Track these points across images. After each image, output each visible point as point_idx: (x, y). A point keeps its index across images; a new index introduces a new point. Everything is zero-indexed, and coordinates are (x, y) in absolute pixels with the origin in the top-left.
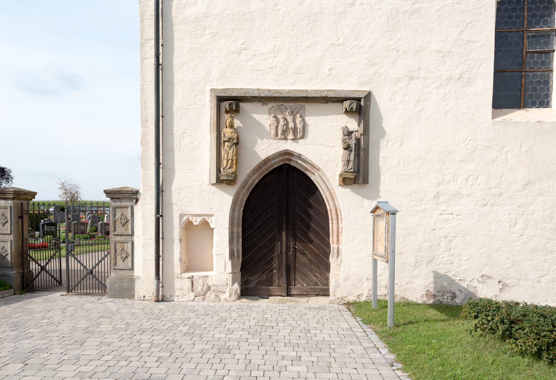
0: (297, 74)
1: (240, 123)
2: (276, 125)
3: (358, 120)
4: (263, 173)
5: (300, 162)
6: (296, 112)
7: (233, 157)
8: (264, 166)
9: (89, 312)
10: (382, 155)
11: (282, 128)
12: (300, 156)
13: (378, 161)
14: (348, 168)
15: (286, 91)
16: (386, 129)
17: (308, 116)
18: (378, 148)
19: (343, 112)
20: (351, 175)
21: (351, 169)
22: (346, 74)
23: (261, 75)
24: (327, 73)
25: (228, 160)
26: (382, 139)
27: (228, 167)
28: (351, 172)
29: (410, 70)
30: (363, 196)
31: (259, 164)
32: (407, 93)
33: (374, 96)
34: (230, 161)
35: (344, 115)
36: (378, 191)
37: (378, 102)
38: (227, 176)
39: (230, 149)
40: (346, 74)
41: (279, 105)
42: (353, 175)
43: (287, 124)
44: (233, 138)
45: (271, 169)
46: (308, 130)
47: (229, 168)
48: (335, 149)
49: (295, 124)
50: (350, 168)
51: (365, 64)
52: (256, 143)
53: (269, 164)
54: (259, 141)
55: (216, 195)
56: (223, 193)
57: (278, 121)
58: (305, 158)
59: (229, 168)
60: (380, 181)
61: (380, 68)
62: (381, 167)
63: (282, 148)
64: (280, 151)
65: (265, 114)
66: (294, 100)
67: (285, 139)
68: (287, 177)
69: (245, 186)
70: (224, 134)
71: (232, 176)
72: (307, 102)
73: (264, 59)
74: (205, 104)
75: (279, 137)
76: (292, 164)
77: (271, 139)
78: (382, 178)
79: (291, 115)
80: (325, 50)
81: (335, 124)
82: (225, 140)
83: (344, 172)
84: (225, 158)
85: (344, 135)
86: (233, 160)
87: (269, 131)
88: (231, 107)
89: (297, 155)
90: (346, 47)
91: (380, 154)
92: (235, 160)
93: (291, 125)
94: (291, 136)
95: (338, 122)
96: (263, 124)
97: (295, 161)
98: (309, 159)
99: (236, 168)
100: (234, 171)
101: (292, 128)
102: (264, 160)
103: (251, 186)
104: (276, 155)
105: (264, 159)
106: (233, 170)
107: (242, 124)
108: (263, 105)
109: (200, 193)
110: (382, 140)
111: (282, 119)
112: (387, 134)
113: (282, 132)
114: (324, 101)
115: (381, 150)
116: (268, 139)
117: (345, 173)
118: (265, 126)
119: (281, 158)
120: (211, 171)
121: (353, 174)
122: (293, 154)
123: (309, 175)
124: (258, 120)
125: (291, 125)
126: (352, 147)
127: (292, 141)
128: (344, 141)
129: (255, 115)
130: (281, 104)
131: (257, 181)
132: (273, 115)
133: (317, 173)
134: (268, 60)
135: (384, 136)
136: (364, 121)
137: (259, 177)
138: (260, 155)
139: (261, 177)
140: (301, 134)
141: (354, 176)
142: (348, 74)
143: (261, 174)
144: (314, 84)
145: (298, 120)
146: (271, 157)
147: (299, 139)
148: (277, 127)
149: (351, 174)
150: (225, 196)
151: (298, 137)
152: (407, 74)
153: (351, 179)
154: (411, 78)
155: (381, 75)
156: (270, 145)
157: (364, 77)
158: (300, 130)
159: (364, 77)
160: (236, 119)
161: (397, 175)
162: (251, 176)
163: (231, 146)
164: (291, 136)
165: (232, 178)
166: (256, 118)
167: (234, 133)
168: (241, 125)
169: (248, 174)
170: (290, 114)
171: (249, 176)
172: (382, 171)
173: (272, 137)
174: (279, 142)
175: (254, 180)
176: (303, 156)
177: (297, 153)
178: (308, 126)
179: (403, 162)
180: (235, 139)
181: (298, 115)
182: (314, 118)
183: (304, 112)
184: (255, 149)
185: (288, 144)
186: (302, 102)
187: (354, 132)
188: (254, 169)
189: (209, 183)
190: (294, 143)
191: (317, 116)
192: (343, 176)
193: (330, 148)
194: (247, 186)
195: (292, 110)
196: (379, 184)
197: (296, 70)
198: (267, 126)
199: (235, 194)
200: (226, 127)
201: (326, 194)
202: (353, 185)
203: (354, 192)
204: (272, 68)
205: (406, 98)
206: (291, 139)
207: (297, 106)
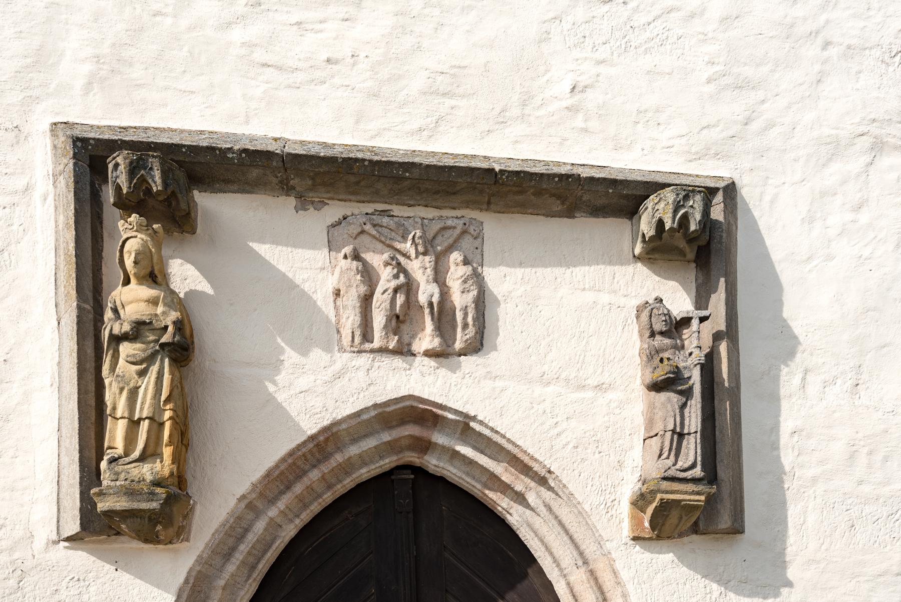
0: (444, 95)
1: (201, 278)
2: (363, 289)
3: (694, 285)
4: (316, 499)
5: (466, 451)
6: (446, 244)
7: (158, 409)
8: (314, 466)
9: (854, 447)
10: (787, 425)
11: (387, 305)
12: (467, 425)
13: (775, 446)
14: (680, 464)
15: (401, 152)
16: (797, 328)
17: (493, 266)
18: (774, 399)
19: (638, 250)
20: (693, 493)
21: (693, 466)
22: (639, 112)
23: (289, 86)
24: (565, 104)
25: (134, 424)
26: (787, 366)
27: (136, 454)
28: (694, 480)
29: (872, 116)
30: (724, 582)
31: (291, 454)
32: (867, 200)
33: (746, 204)
34: (145, 425)
35: (639, 265)
36: (780, 563)
37: (761, 228)
38: (130, 492)
39: (142, 373)
40: (639, 112)
41: (370, 211)
42: (698, 493)
43: (408, 288)
44: (156, 324)
45: (348, 483)
46: (498, 320)
47: (142, 459)
48: (611, 395)
49: (445, 293)
50: (689, 463)
51: (709, 81)
52: (276, 365)
53: (339, 458)
54: (290, 356)
55: (91, 589)
56: (125, 577)
57: (368, 276)
58: (487, 432)
59: (142, 459)
60: (784, 521)
61: (763, 102)
62: (787, 468)
63: (389, 387)
64: (380, 400)
65: (313, 247)
66: (437, 192)
67: (404, 351)
68: (411, 515)
69: (233, 549)
70: (115, 311)
71: (152, 493)
72: (488, 206)
73: (299, 24)
74: (27, 189)
75: (377, 344)
76: (433, 463)
77: (342, 349)
78: (793, 512)
79: (425, 254)
80: (551, 15)
81: (605, 298)
82: (116, 331)
83: (665, 479)
84: (119, 415)
85: (653, 335)
86: (162, 424)
87: (333, 319)
88: (143, 180)
89: (456, 422)
90: (636, 10)
91: (782, 419)
92: (168, 425)
93: (427, 292)
94: (427, 340)
95: (615, 292)
96: (306, 287)
97: (443, 447)
98: (504, 437)
99: (177, 459)
100: (166, 472)
101: (431, 304)
102: (312, 438)
103: (265, 551)
104: (365, 417)
105: (314, 431)
106: (164, 465)
107: (209, 282)
108: (303, 203)
109: (12, 582)
110: (785, 370)
111: (387, 264)
112: (800, 348)
113: (389, 320)
114: (557, 207)
115: (785, 404)
116: (328, 349)
117: (665, 485)
118: (314, 297)
119: (386, 437)
120: (64, 483)
121: (700, 488)
122: (436, 417)
123: (502, 503)
124: (282, 268)
125: (429, 292)
126: (689, 378)
127: (431, 363)
128: (653, 356)
129: (267, 246)
130: (381, 207)
131: (290, 532)
132: (347, 250)
133: (539, 496)
134: (321, 31)
135: (791, 353)
136: (726, 281)
137: (298, 516)
138: (293, 414)
139: (306, 516)
140: (471, 331)
141: (703, 498)
142: (646, 111)
143: (303, 502)
144: (516, 142)
145: (456, 273)
146: (344, 426)
147: (460, 355)
148: (367, 300)
149: (690, 487)
150: (136, 591)
151: (458, 345)
152: (863, 129)
153: (690, 508)
154: (879, 147)
155: (770, 125)
156: (338, 376)
157: (708, 127)
158: (466, 315)
159: (708, 127)
160: (179, 261)
161: (850, 501)
162: (259, 505)
163: (150, 359)
164: (427, 340)
165: (154, 505)
166: (274, 263)
167: (165, 305)
168: (204, 286)
169: (243, 497)
170: (421, 249)
171: (250, 506)
172: (791, 486)
173: (346, 340)
174: (376, 364)
175: (274, 526)
176: (481, 423)
177: (456, 412)
178: (497, 302)
179: (866, 450)
180: (171, 329)
181: (456, 257)
182: (519, 272)
183: (480, 249)
184: (271, 388)
185: (415, 373)
186: (468, 205)
187: (695, 323)
188: (269, 474)
189: (54, 537)
190: (443, 372)
191: (532, 266)
192: (659, 496)
193: (589, 394)
194: (243, 548)
195: (430, 235)
196: (781, 536)
197: (440, 78)
198: (323, 298)
199: (187, 581)
200: (127, 282)
201: (572, 579)
202: (686, 539)
203: (689, 567)
204: (336, 62)
205: (864, 217)
206: (428, 354)
207: (449, 223)
